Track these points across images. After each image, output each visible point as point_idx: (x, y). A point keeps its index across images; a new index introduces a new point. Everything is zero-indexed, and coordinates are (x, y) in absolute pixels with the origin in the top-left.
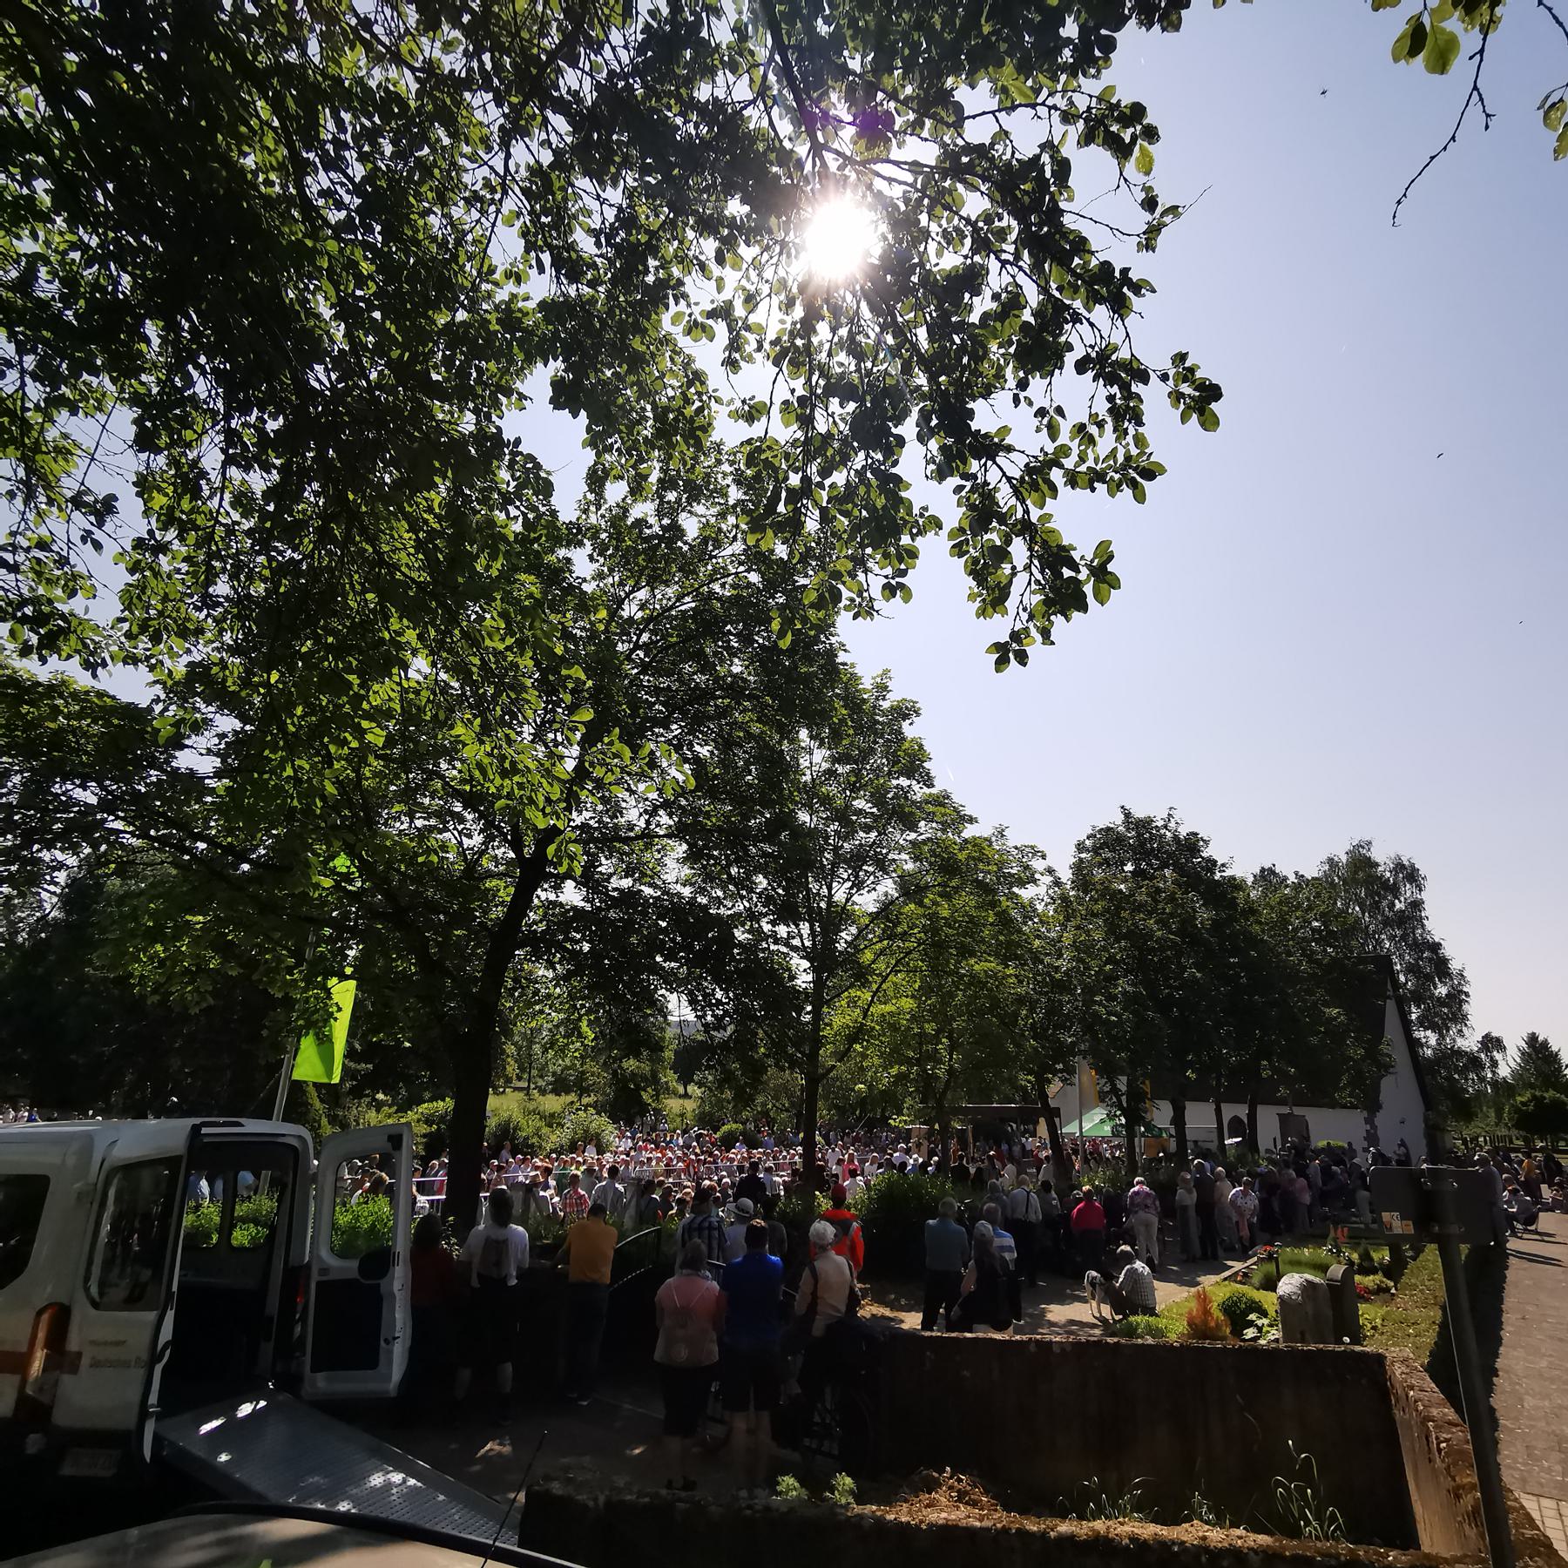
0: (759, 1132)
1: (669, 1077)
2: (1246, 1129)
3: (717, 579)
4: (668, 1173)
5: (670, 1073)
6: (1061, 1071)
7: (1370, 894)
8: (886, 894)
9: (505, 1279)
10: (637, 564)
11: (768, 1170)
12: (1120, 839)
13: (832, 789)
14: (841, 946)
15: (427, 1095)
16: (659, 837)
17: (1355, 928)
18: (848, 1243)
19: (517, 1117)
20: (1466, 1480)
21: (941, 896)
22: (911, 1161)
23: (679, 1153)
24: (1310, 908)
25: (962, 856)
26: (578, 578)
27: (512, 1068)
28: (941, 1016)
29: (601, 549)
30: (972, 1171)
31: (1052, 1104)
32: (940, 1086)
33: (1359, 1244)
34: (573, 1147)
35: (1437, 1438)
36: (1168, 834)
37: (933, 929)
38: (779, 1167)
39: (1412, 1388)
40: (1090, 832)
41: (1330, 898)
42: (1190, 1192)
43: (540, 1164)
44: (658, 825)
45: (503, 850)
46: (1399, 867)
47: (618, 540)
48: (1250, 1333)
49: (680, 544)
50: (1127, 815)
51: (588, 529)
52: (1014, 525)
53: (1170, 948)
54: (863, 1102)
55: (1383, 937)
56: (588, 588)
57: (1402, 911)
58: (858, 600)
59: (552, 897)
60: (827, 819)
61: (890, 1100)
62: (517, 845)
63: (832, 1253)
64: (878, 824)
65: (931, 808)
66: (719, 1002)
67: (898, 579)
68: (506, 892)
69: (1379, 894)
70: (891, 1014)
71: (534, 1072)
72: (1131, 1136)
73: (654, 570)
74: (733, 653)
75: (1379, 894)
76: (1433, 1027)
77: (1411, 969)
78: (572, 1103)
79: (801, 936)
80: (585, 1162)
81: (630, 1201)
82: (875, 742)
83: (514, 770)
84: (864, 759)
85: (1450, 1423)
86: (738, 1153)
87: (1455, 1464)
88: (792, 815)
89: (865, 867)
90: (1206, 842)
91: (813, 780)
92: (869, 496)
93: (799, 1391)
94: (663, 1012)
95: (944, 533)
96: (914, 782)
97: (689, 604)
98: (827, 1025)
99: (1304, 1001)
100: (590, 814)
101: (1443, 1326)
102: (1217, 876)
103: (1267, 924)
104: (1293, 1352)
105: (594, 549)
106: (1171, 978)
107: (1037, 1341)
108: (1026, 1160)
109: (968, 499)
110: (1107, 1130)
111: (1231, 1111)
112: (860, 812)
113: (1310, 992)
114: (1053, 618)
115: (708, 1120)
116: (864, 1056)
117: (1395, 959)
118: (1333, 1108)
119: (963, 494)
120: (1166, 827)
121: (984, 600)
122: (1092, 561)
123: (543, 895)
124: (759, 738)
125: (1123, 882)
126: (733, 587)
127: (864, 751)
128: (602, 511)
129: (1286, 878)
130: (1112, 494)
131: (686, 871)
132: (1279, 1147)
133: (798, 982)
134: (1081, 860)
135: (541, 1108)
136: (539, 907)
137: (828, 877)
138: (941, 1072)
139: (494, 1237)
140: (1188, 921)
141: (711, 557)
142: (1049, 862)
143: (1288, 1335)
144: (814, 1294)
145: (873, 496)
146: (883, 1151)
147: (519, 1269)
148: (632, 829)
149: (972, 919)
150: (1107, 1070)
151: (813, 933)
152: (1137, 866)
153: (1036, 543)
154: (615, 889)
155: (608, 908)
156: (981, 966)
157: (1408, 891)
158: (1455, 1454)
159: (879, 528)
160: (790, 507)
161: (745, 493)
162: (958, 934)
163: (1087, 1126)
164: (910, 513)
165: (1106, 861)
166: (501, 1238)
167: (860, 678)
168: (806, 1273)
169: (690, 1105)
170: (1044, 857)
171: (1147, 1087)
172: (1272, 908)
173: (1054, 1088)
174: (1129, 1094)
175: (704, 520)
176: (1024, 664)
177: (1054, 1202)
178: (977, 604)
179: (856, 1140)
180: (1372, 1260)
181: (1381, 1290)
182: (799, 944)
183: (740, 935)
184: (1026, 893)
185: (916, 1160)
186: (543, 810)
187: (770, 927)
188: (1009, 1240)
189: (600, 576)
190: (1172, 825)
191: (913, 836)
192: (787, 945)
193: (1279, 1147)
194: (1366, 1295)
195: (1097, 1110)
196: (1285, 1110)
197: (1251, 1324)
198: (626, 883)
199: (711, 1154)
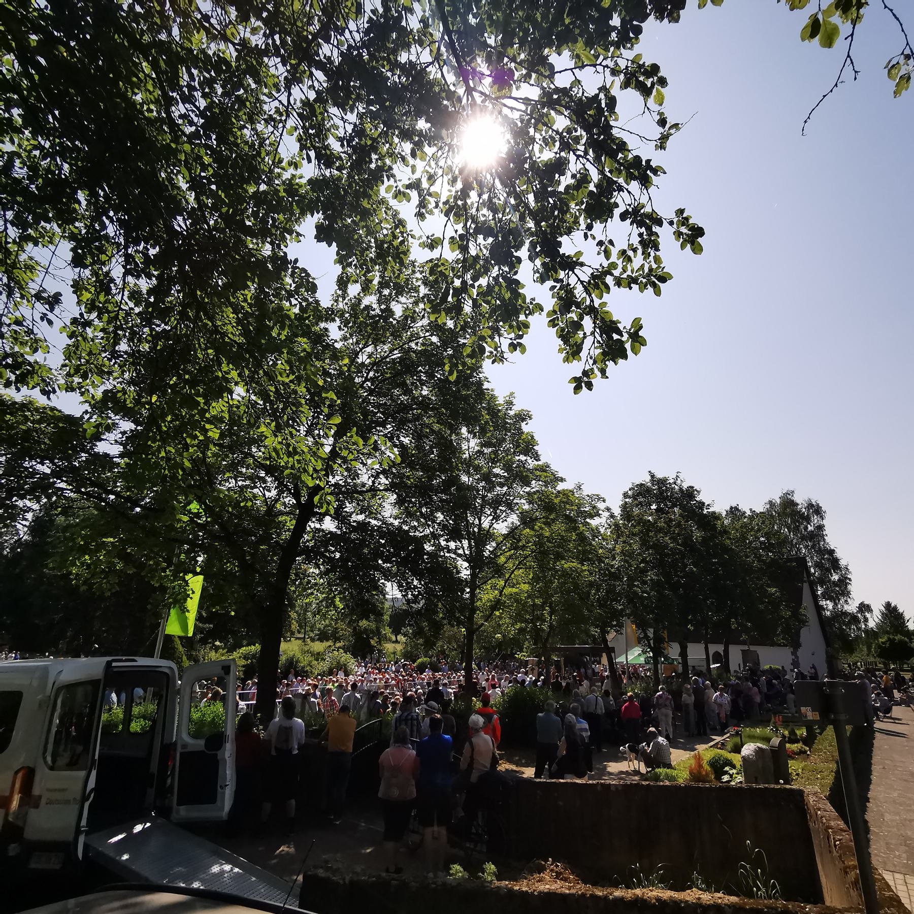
0: (440, 662)
1: (387, 631)
2: (722, 659)
3: (413, 340)
4: (386, 687)
5: (387, 628)
6: (615, 626)
7: (793, 521)
9: (290, 751)
10: (366, 332)
11: (445, 685)
13: (481, 462)
14: (487, 553)
16: (380, 490)
17: (785, 541)
18: (491, 727)
23: (393, 675)
24: (759, 530)
25: (556, 501)
27: (295, 626)
28: (545, 593)
29: (346, 323)
30: (564, 684)
31: (610, 645)
32: (545, 635)
33: (788, 726)
34: (331, 672)
35: (834, 839)
36: (676, 487)
37: (539, 544)
38: (451, 683)
39: (819, 809)
41: (770, 524)
42: (689, 695)
43: (311, 682)
45: (289, 498)
46: (810, 505)
47: (355, 317)
49: (391, 320)
50: (653, 476)
52: (585, 309)
53: (678, 554)
54: (500, 644)
55: (801, 546)
56: (338, 345)
57: (812, 531)
58: (495, 352)
59: (318, 526)
61: (516, 644)
62: (297, 496)
65: (538, 473)
66: (415, 587)
67: (518, 340)
68: (291, 524)
69: (798, 522)
71: (308, 629)
72: (656, 663)
75: (798, 522)
76: (831, 599)
77: (817, 565)
78: (330, 646)
80: (337, 681)
81: (364, 704)
84: (499, 445)
85: (842, 830)
86: (427, 675)
89: (500, 508)
90: (699, 492)
92: (501, 292)
93: (463, 814)
96: (529, 458)
97: (397, 355)
101: (837, 772)
102: (705, 512)
105: (341, 323)
107: (602, 784)
108: (594, 678)
109: (558, 294)
110: (642, 660)
112: (497, 475)
113: (759, 579)
114: (607, 363)
115: (410, 656)
116: (500, 618)
117: (808, 559)
119: (555, 290)
120: (675, 483)
121: (568, 353)
122: (630, 330)
123: (312, 525)
124: (438, 433)
125: (650, 515)
126: (423, 344)
128: (346, 301)
129: (745, 513)
131: (395, 511)
134: (626, 503)
137: (479, 514)
138: (545, 627)
139: (284, 725)
141: (410, 327)
142: (607, 504)
144: (472, 758)
146: (512, 673)
147: (299, 744)
150: (642, 625)
152: (659, 506)
154: (354, 521)
157: (815, 519)
159: (507, 310)
160: (455, 299)
161: (429, 290)
162: (555, 546)
163: (630, 658)
164: (524, 302)
165: (641, 503)
167: (497, 397)
169: (399, 647)
170: (604, 501)
172: (737, 530)
173: (611, 635)
174: (655, 639)
175: (405, 306)
176: (591, 390)
178: (564, 355)
179: (496, 666)
180: (796, 734)
181: (802, 752)
182: (462, 553)
183: (428, 547)
184: (594, 522)
185: (531, 678)
186: (312, 476)
187: (445, 542)
188: (585, 725)
189: (345, 339)
190: (679, 482)
191: (528, 489)
192: (455, 553)
194: (793, 755)
195: (637, 648)
196: (746, 648)
197: (726, 773)
198: (361, 517)
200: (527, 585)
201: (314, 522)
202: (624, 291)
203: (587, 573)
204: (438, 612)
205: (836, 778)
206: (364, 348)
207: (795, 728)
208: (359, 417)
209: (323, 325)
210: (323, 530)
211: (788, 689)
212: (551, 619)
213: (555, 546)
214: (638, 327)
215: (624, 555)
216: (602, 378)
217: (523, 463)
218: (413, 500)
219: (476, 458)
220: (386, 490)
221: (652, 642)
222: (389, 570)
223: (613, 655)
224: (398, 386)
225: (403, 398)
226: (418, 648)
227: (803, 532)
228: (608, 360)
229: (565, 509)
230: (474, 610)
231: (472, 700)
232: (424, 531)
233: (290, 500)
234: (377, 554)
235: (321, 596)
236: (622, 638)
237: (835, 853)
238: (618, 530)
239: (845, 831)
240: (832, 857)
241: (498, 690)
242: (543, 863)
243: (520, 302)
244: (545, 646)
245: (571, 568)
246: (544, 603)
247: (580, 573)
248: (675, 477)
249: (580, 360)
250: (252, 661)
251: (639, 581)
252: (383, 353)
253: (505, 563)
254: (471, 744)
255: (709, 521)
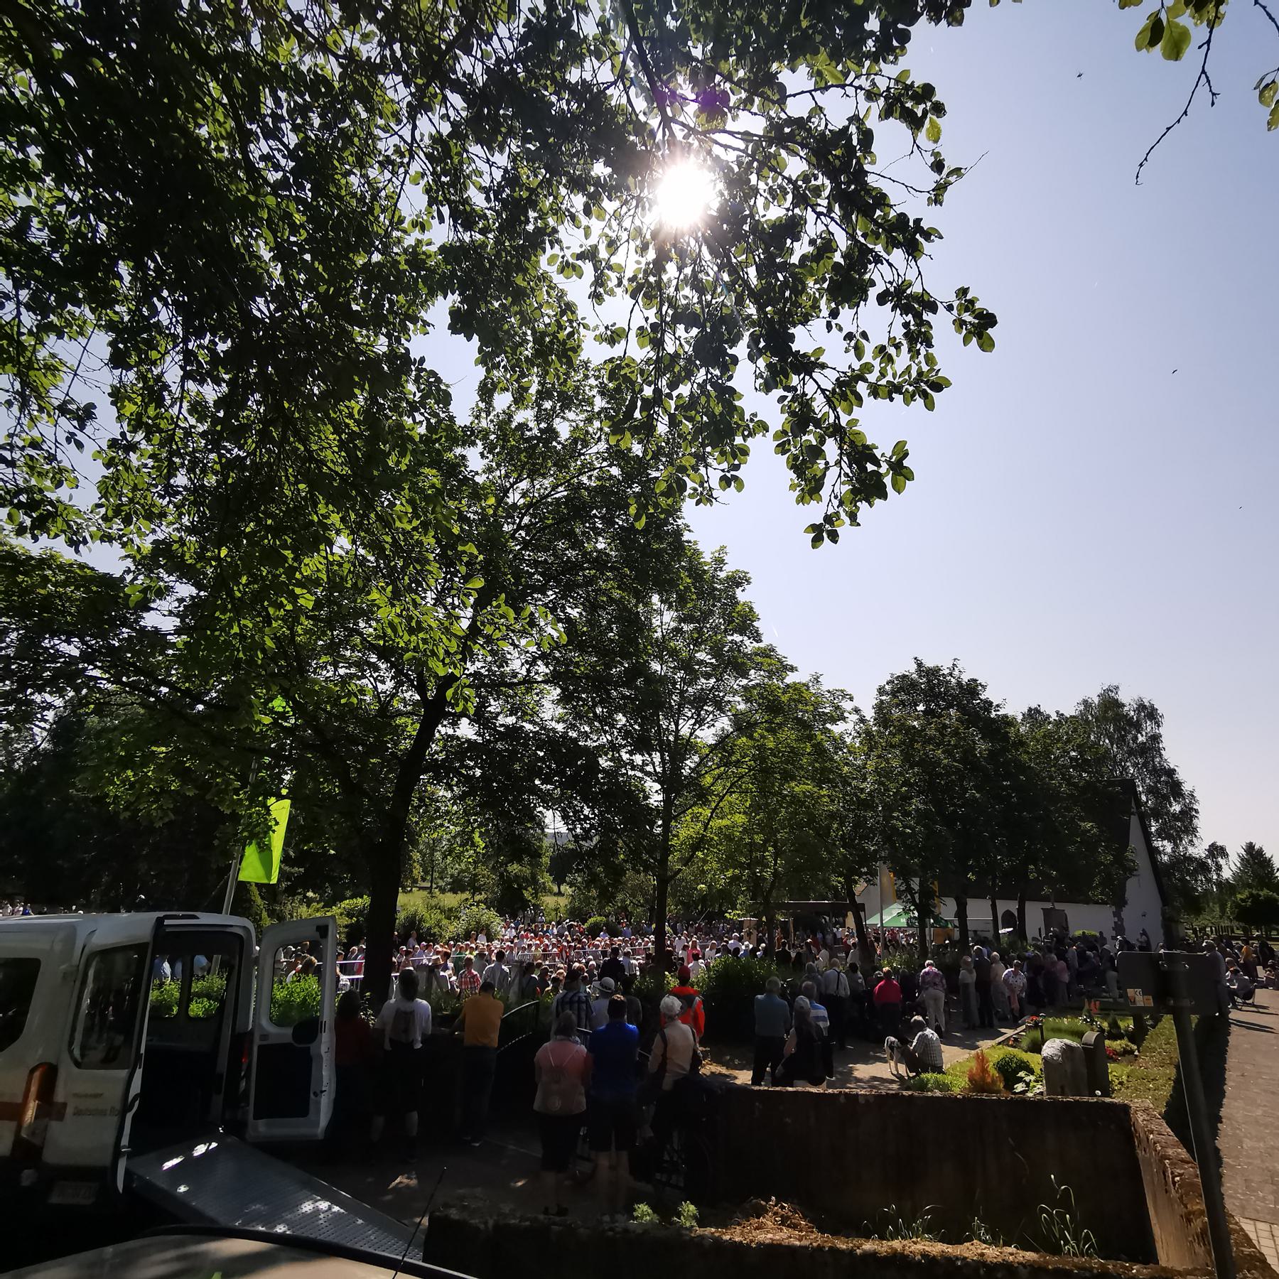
0: (619, 923)
1: (546, 879)
2: (1017, 921)
3: (585, 473)
4: (545, 957)
5: (547, 875)
6: (866, 874)
7: (1117, 729)
8: (723, 729)
9: (412, 1043)
10: (520, 460)
11: (627, 954)
12: (914, 684)
13: (678, 644)
14: (686, 772)
15: (348, 893)
16: (538, 682)
17: (1105, 757)
18: (692, 1014)
19: (422, 911)
20: (1196, 1208)
21: (767, 731)
22: (743, 947)
23: (554, 941)
24: (1068, 741)
25: (784, 698)
26: (471, 471)
27: (417, 871)
28: (767, 829)
29: (490, 448)
30: (793, 955)
31: (858, 900)
32: (767, 886)
33: (1108, 1015)
34: (467, 936)
35: (1172, 1173)
36: (953, 680)
37: (761, 758)
38: (635, 952)
39: (1152, 1132)
40: (889, 678)
41: (1085, 732)
42: (970, 972)
43: (440, 949)
44: (537, 673)
45: (410, 693)
46: (1141, 707)
47: (504, 440)
48: (1020, 1087)
49: (554, 443)
50: (920, 665)
51: (480, 432)
52: (827, 428)
53: (954, 773)
54: (704, 899)
55: (1128, 764)
56: (480, 479)
57: (1143, 743)
58: (700, 489)
59: (450, 731)
60: (675, 668)
61: (726, 897)
62: (421, 689)
63: (679, 1022)
64: (716, 672)
65: (759, 659)
66: (587, 817)
67: (732, 473)
68: (413, 728)
69: (1125, 730)
70: (727, 827)
71: (436, 875)
72: (922, 927)
73: (533, 465)
74: (598, 533)
75: (1125, 730)
76: (1169, 838)
77: (1151, 791)
78: (467, 899)
79: (653, 764)
80: (477, 948)
81: (514, 980)
82: (714, 606)
83: (420, 628)
84: (705, 619)
85: (1183, 1161)
86: (602, 940)
87: (1187, 1194)
88: (646, 665)
89: (705, 708)
90: (984, 687)
91: (663, 636)
92: (709, 404)
93: (652, 1135)
94: (541, 825)
95: (770, 434)
96: (746, 638)
97: (562, 493)
98: (674, 836)
99: (1064, 817)
100: (481, 664)
101: (1177, 1082)
102: (993, 715)
103: (1034, 754)
104: (1055, 1103)
105: (484, 448)
106: (955, 798)
107: (846, 1094)
108: (837, 946)
109: (790, 407)
110: (903, 921)
111: (1004, 906)
112: (701, 662)
113: (1068, 809)
114: (859, 504)
115: (577, 914)
116: (705, 861)
117: (1138, 782)
118: (1087, 903)
119: (786, 403)
120: (951, 674)
121: (802, 490)
122: (891, 458)
123: (443, 730)
124: (619, 602)
125: (916, 720)
126: (598, 478)
127: (705, 613)
128: (491, 417)
129: (1049, 717)
130: (907, 403)
131: (560, 711)
132: (1043, 936)
133: (651, 801)
134: (882, 701)
135: (441, 904)
136: (439, 740)
137: (676, 715)
138: (768, 874)
139: (403, 1009)
140: (969, 752)
141: (580, 454)
142: (856, 703)
143: (1051, 1089)
144: (664, 1056)
145: (712, 404)
146: (720, 939)
147: (423, 1035)
148: (515, 677)
149: (792, 750)
150: (903, 873)
151: (663, 761)
152: (928, 706)
153: (845, 443)
154: (502, 725)
155: (496, 741)
156: (801, 788)
157: (1148, 727)
158: (1186, 1186)
159: (717, 431)
161: (608, 402)
162: (781, 762)
163: (886, 918)
164: (742, 418)
165: (902, 702)
166: (409, 1010)
167: (702, 553)
168: (658, 1038)
169: (563, 902)
170: (851, 699)
171: (936, 887)
172: (1038, 741)
173: (860, 887)
174: (921, 892)
175: (574, 424)
176: (835, 542)
177: (860, 981)
178: (797, 493)
179: (698, 929)
180: (1119, 1027)
181: (1127, 1052)
182: (652, 770)
183: (604, 762)
184: (837, 729)
185: (747, 946)
186: (443, 661)
187: (628, 756)
188: (823, 1012)
189: (489, 470)
190: (956, 673)
191: (744, 682)
192: (642, 770)
193: (1043, 936)
194: (1114, 1056)
195: (895, 905)
196: (1049, 905)
197: (1020, 1080)
198: (511, 720)
199: (580, 942)
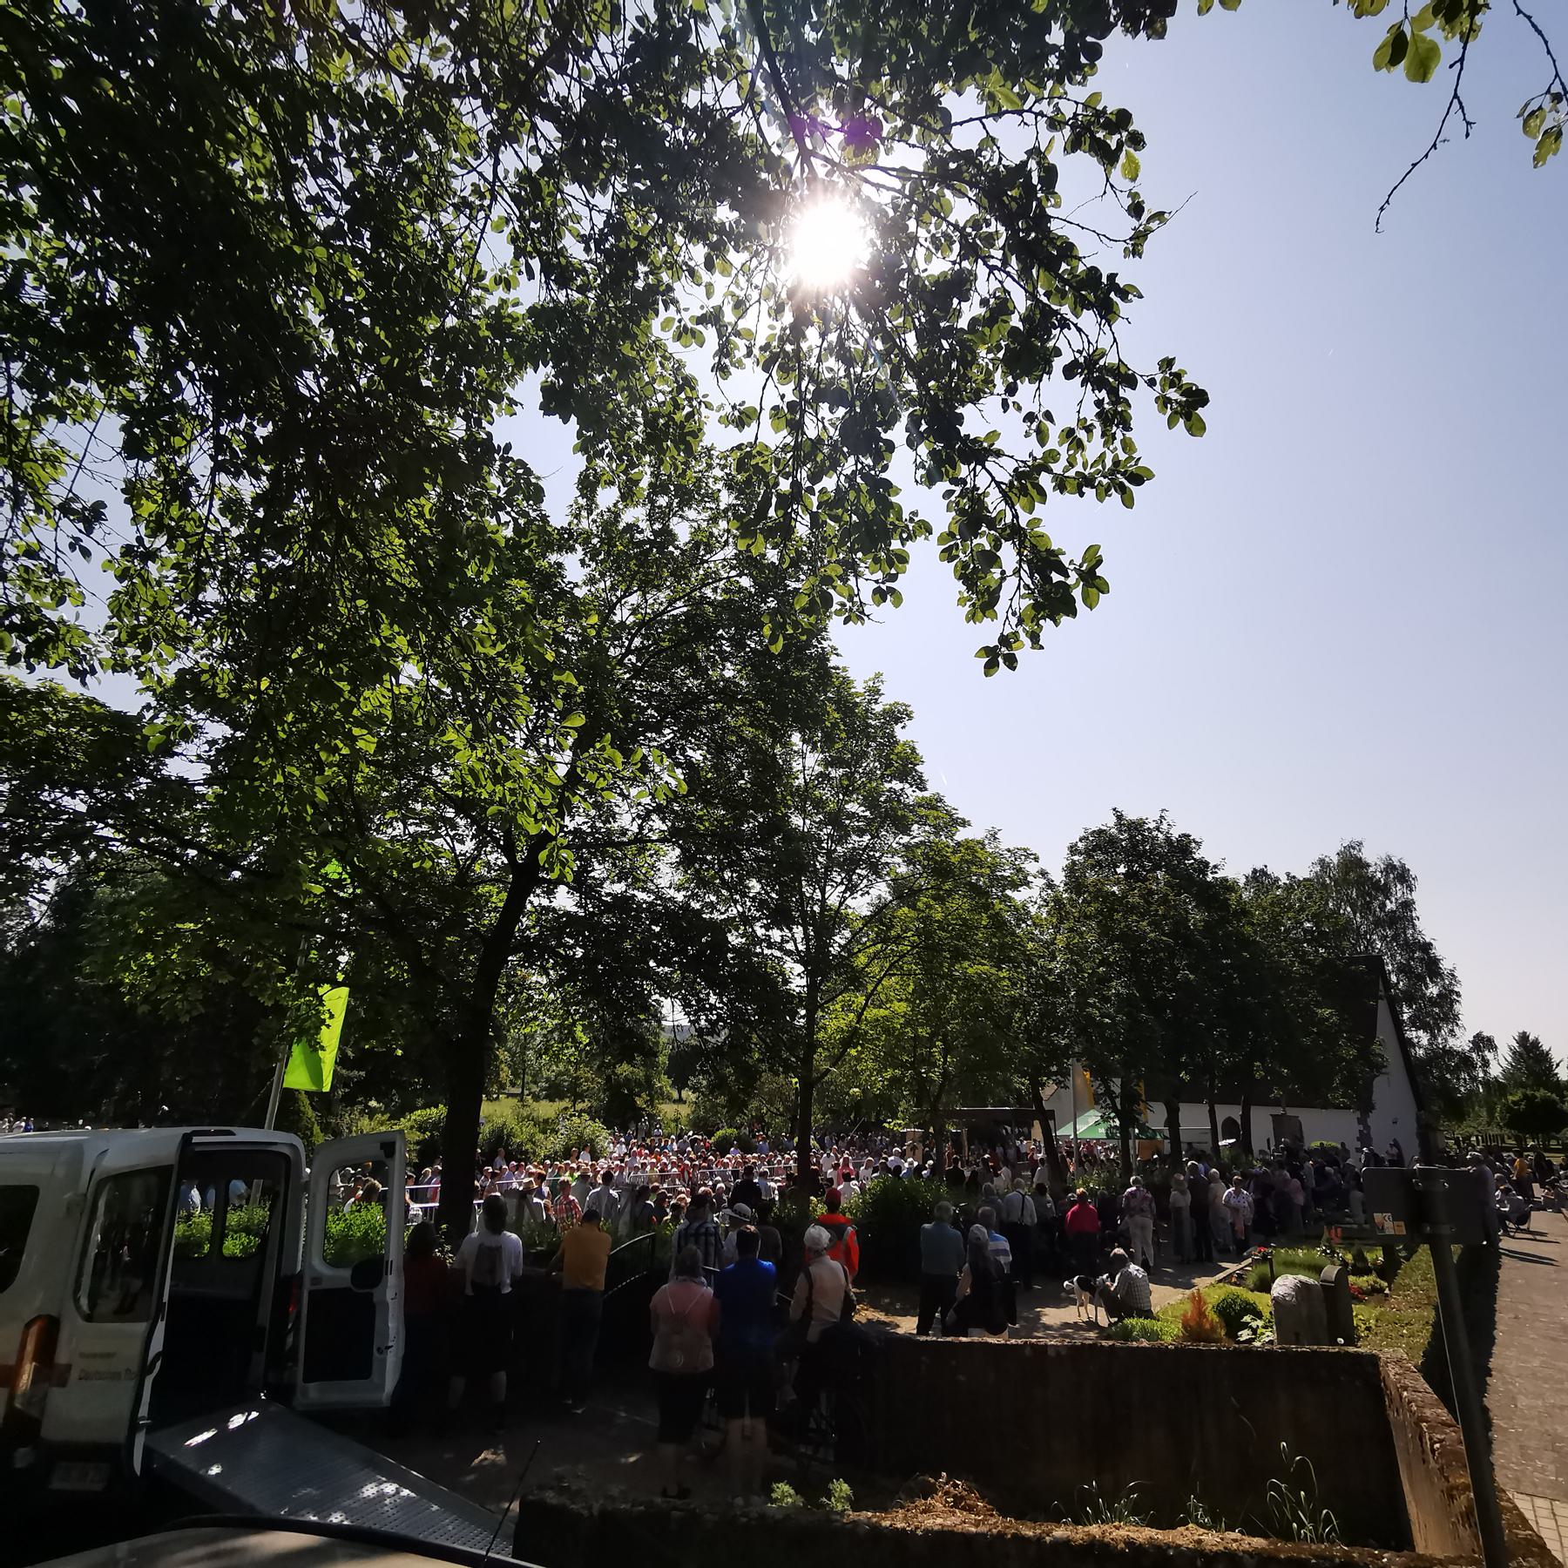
0: (754, 1136)
1: (664, 1082)
2: (1239, 1130)
3: (709, 584)
4: (662, 1179)
5: (663, 1077)
6: (1055, 1074)
7: (1361, 894)
9: (498, 1288)
10: (629, 569)
11: (763, 1175)
13: (826, 793)
14: (835, 950)
15: (420, 1102)
16: (653, 841)
17: (1347, 928)
18: (843, 1247)
23: (674, 1158)
24: (1302, 909)
25: (955, 859)
27: (505, 1074)
28: (934, 1018)
29: (593, 554)
30: (967, 1174)
31: (1047, 1106)
32: (934, 1090)
33: (1353, 1245)
34: (567, 1153)
35: (1431, 1439)
36: (1160, 835)
37: (925, 933)
38: (773, 1172)
39: (1405, 1388)
41: (1322, 898)
42: (1183, 1193)
43: (533, 1170)
45: (495, 855)
46: (1390, 867)
47: (609, 545)
48: (1245, 1335)
49: (671, 548)
50: (1120, 817)
52: (1004, 530)
53: (1162, 950)
54: (857, 1105)
55: (1375, 937)
56: (579, 593)
57: (1393, 912)
58: (849, 605)
59: (545, 902)
61: (886, 1104)
62: (509, 850)
65: (923, 812)
66: (713, 1007)
67: (888, 584)
68: (499, 898)
69: (1370, 895)
71: (528, 1078)
72: (1125, 1137)
75: (1370, 895)
76: (1425, 1027)
77: (1402, 969)
78: (566, 1109)
80: (579, 1168)
81: (625, 1207)
84: (857, 763)
85: (1444, 1424)
86: (733, 1157)
89: (858, 871)
90: (1198, 844)
92: (859, 501)
93: (794, 1397)
96: (907, 786)
97: (680, 608)
101: (1436, 1325)
102: (1210, 878)
104: (1288, 1354)
105: (585, 554)
107: (1032, 1345)
108: (1020, 1163)
109: (957, 504)
110: (1101, 1132)
111: (1224, 1112)
112: (852, 816)
113: (1302, 993)
114: (1042, 622)
115: (703, 1125)
116: (858, 1059)
117: (1386, 959)
119: (953, 498)
120: (1158, 829)
121: (974, 605)
122: (1081, 566)
123: (536, 901)
124: (751, 743)
126: (726, 591)
128: (594, 516)
129: (1277, 880)
131: (678, 877)
134: (1074, 862)
137: (821, 881)
138: (935, 1076)
139: (487, 1243)
141: (703, 561)
142: (1042, 865)
144: (809, 1300)
146: (878, 1155)
147: (513, 1277)
150: (1101, 1072)
152: (1130, 867)
157: (1399, 891)
159: (869, 532)
160: (781, 513)
161: (736, 498)
162: (951, 938)
163: (1081, 1128)
164: (899, 518)
165: (1099, 863)
167: (853, 682)
169: (685, 1110)
170: (1036, 860)
172: (1264, 910)
173: (1049, 1090)
174: (1123, 1096)
175: (695, 525)
176: (1013, 669)
178: (967, 608)
179: (851, 1143)
180: (1365, 1260)
181: (1375, 1291)
182: (793, 948)
183: (734, 939)
184: (1019, 896)
185: (911, 1164)
186: (535, 816)
187: (763, 931)
188: (1004, 1244)
189: (591, 581)
190: (1164, 827)
191: (906, 839)
192: (781, 949)
194: (1360, 1296)
195: (1092, 1112)
196: (1280, 1111)
197: (1246, 1326)
198: (619, 888)
200: (904, 1004)
201: (538, 896)
202: (1071, 499)
203: (1006, 982)
204: (751, 1050)
205: (1434, 1335)
206: (624, 596)
207: (1363, 1248)
208: (616, 715)
209: (553, 557)
210: (554, 910)
211: (1352, 1182)
212: (945, 1062)
213: (951, 938)
214: (1094, 562)
215: (1071, 952)
216: (1033, 648)
217: (898, 795)
218: (709, 857)
219: (816, 786)
220: (662, 840)
221: (1118, 1101)
222: (667, 978)
223: (1051, 1123)
224: (683, 661)
225: (691, 682)
226: (717, 1112)
227: (1378, 913)
228: (1044, 618)
229: (970, 873)
230: (812, 1046)
231: (810, 1202)
232: (727, 910)
233: (497, 858)
234: (648, 951)
235: (551, 1023)
236: (1067, 1095)
237: (1432, 1464)
238: (1060, 908)
239: (1450, 1426)
240: (1428, 1471)
241: (854, 1184)
242: (932, 1480)
243: (892, 517)
244: (934, 1108)
245: (979, 975)
246: (933, 1035)
247: (994, 983)
248: (1157, 818)
249: (994, 617)
250: (432, 1135)
251: (1096, 997)
252: (656, 606)
253: (867, 965)
254: (808, 1276)
255: (1217, 894)
